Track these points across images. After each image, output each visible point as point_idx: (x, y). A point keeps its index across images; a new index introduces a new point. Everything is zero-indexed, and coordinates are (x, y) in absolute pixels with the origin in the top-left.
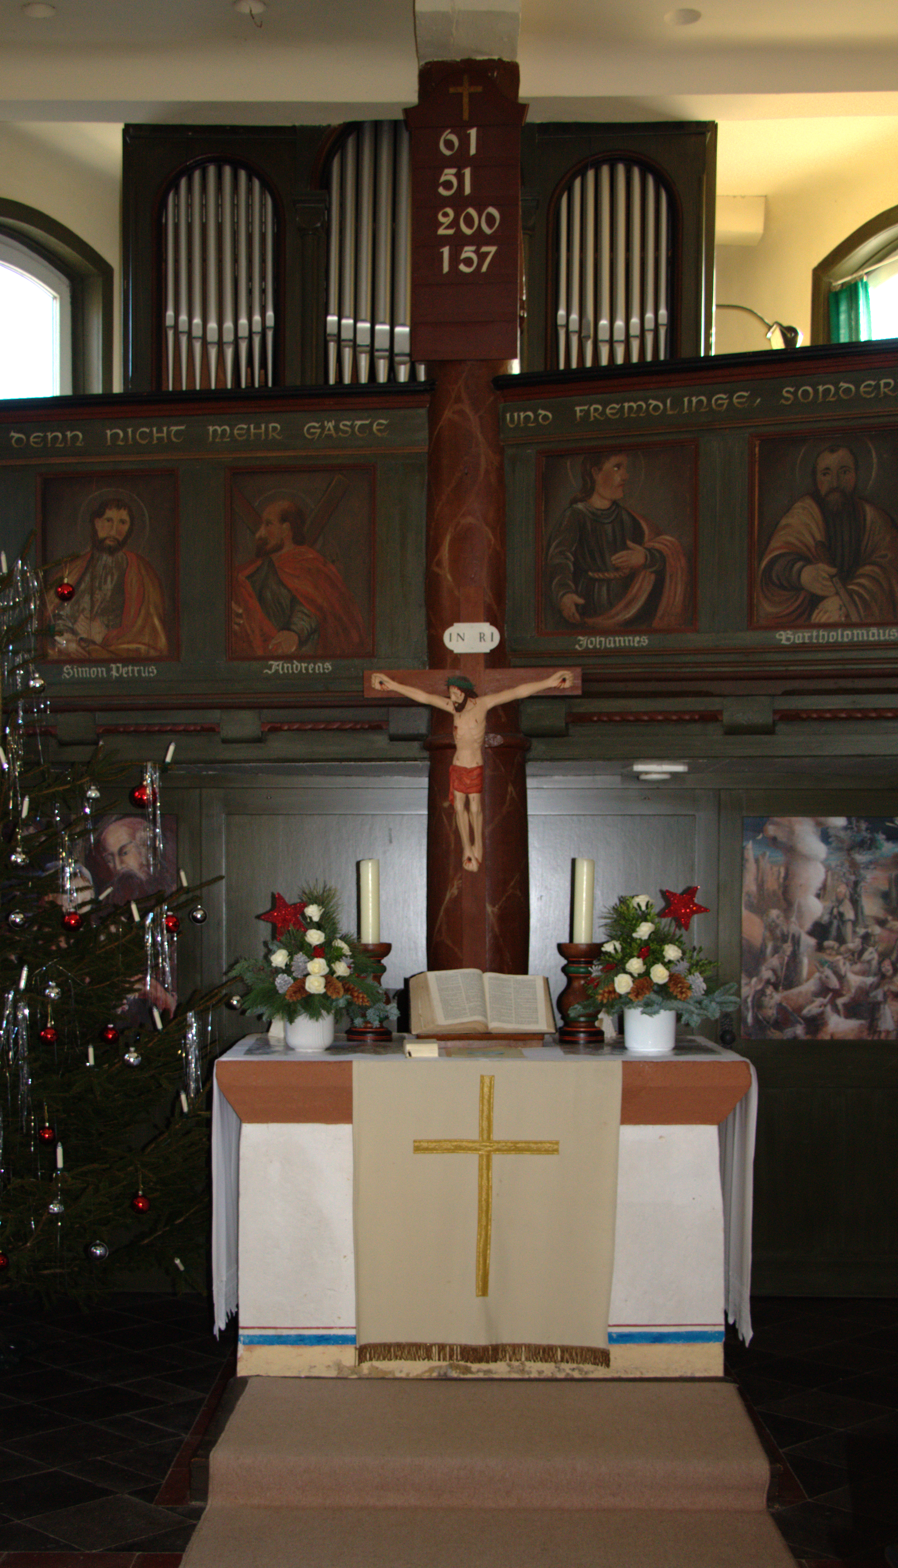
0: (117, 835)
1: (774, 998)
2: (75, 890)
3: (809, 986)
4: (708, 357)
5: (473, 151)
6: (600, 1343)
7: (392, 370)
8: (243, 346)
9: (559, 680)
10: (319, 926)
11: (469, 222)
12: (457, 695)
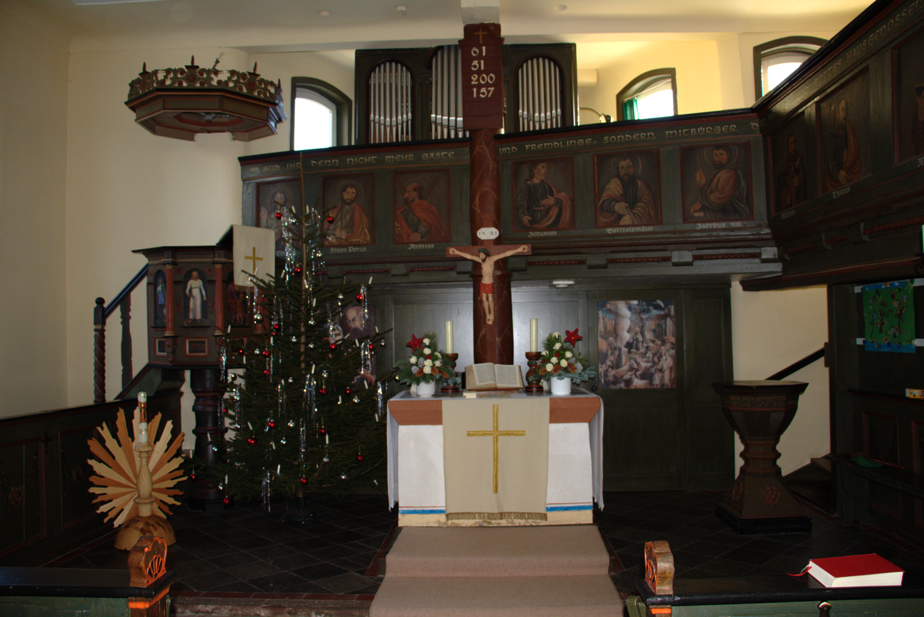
0: (352, 313)
1: (612, 373)
2: (335, 333)
3: (625, 368)
4: (577, 126)
5: (484, 54)
6: (543, 511)
7: (456, 134)
8: (400, 127)
9: (522, 249)
10: (429, 347)
11: (483, 79)
12: (482, 256)
